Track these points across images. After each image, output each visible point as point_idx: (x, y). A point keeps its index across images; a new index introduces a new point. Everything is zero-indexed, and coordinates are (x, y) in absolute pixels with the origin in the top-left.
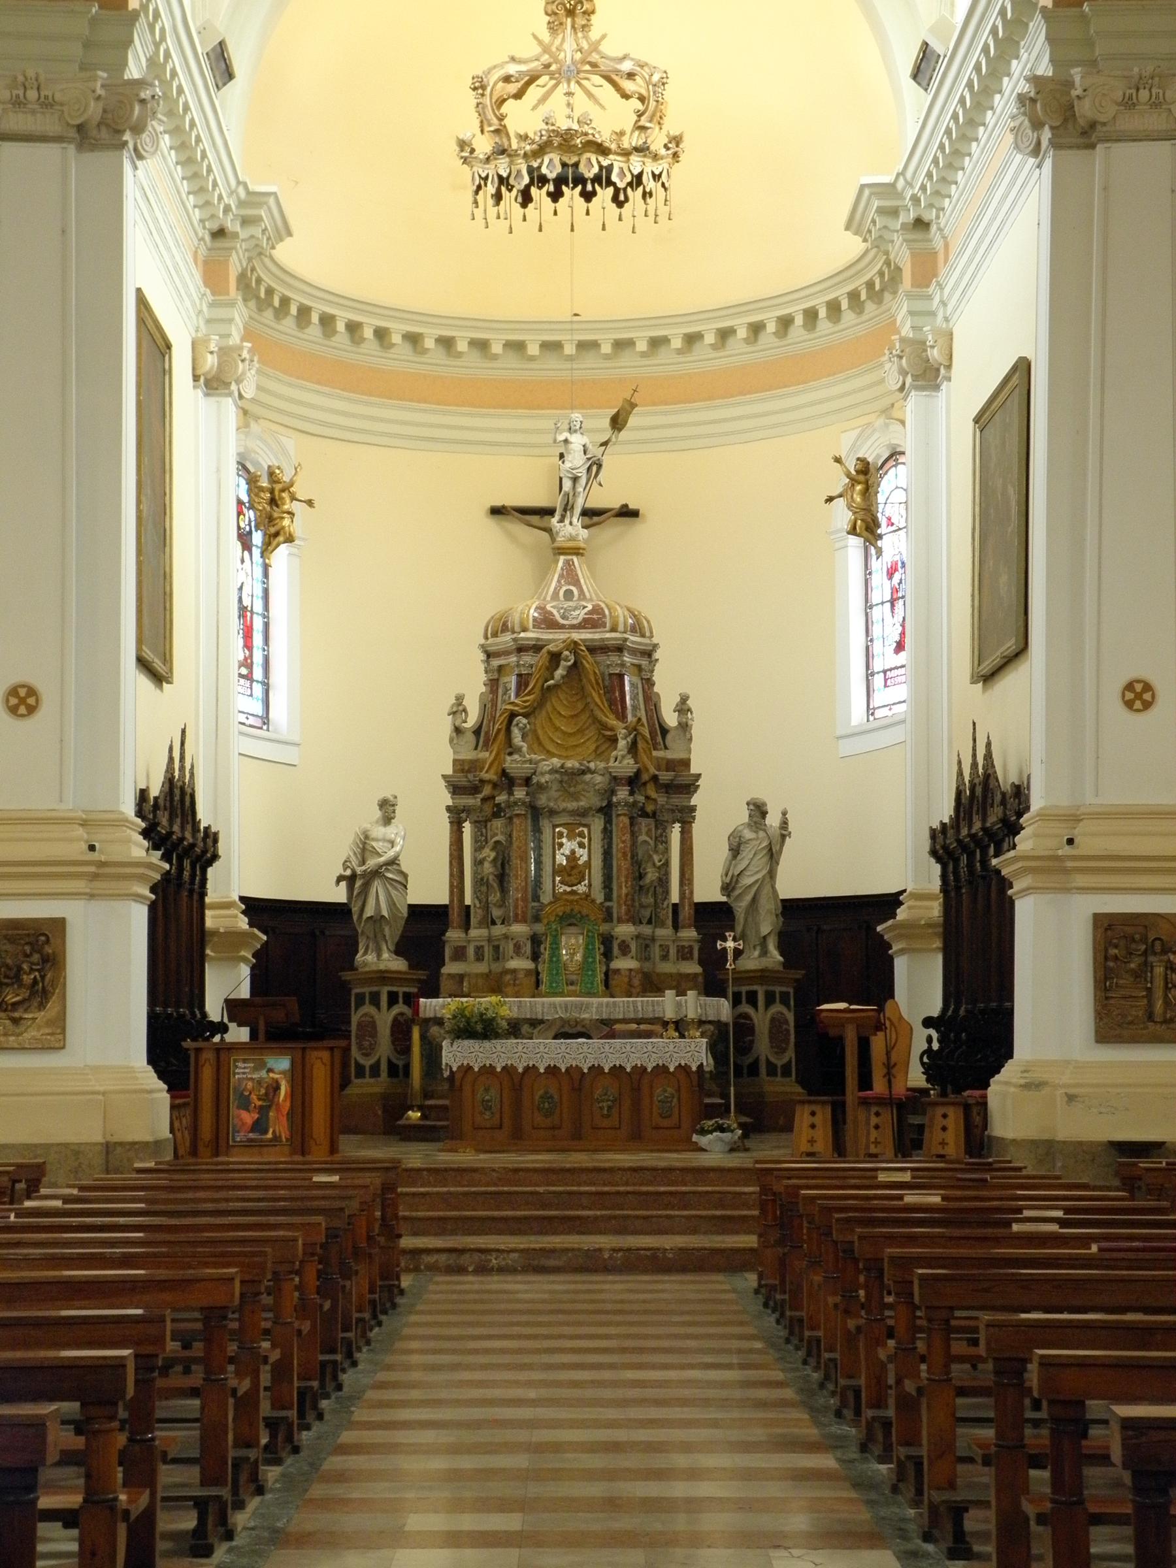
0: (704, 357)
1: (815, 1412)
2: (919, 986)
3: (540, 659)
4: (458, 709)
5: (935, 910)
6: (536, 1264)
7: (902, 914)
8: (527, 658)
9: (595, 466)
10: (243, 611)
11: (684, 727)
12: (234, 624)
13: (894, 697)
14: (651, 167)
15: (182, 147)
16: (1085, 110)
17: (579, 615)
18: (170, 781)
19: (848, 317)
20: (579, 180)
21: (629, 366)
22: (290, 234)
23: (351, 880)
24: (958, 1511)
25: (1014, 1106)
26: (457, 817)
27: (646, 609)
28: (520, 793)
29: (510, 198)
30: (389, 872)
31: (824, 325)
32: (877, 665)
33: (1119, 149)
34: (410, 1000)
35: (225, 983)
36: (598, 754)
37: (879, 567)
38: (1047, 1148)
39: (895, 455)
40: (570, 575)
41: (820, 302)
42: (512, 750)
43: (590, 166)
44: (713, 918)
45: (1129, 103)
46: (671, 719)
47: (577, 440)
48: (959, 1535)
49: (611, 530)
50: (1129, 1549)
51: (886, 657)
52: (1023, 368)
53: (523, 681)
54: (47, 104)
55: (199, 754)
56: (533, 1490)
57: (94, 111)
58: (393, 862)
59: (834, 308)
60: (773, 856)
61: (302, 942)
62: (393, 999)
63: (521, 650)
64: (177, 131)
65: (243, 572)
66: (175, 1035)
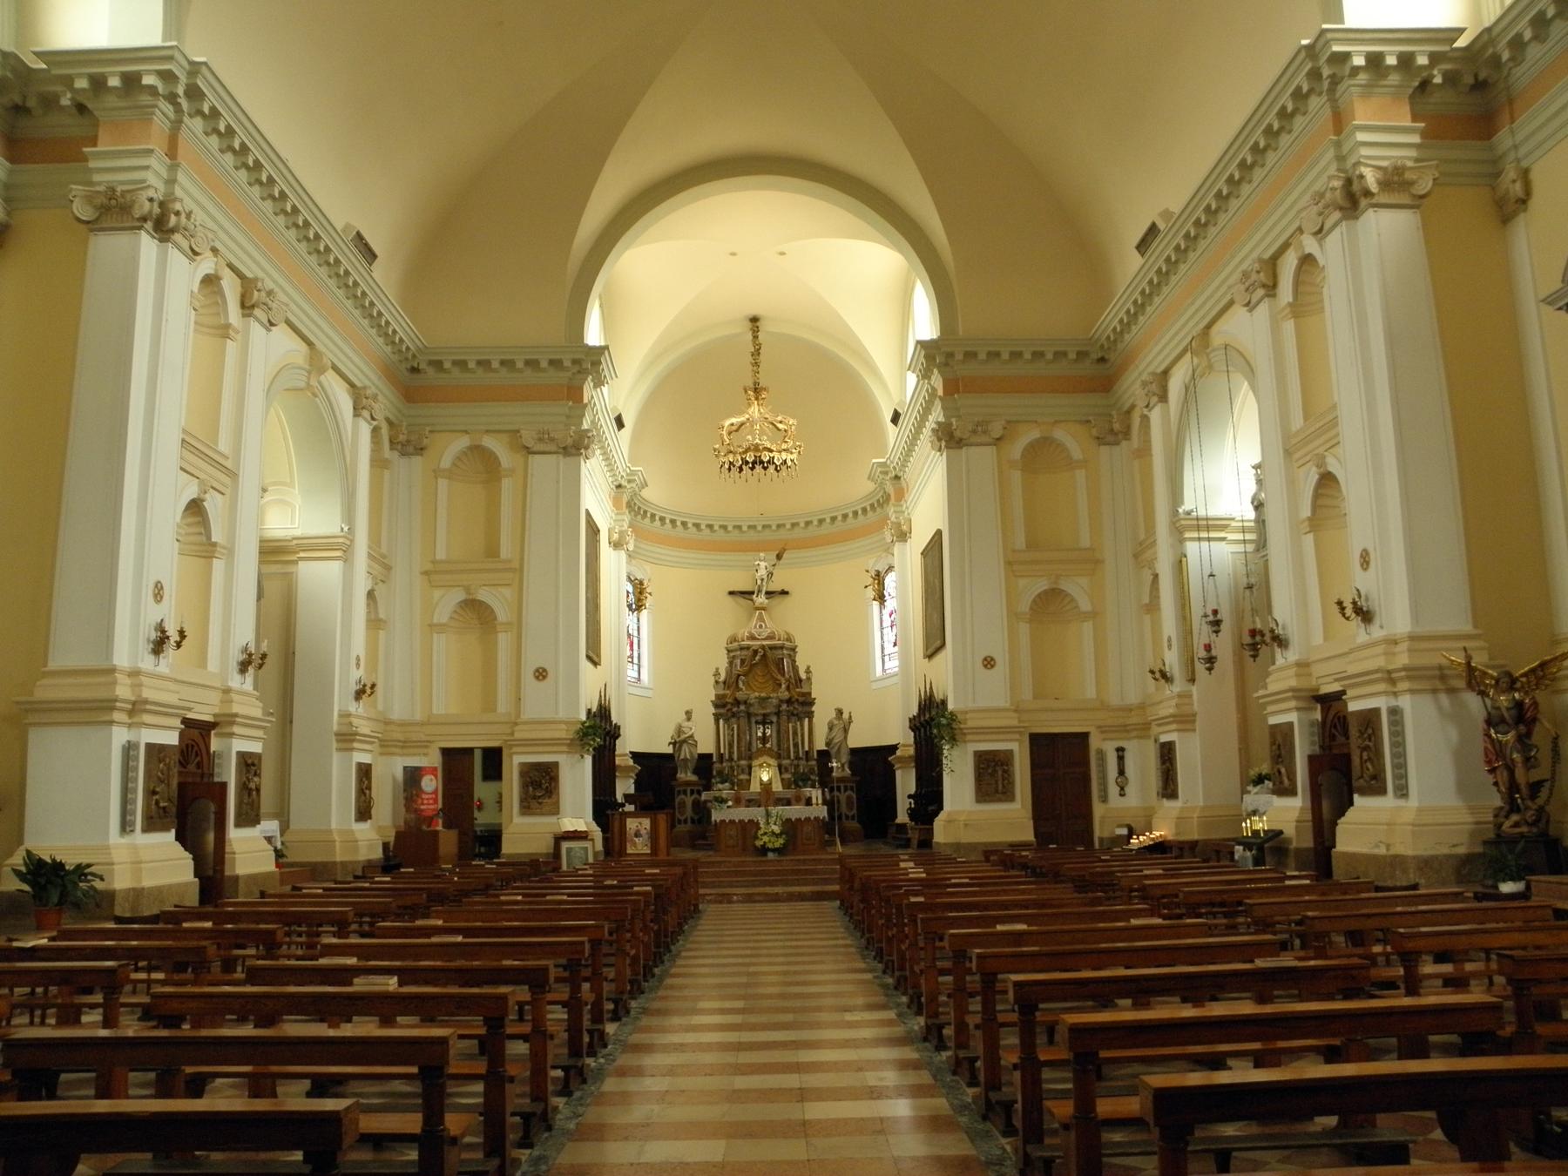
1: (864, 958)
2: (906, 783)
3: (749, 653)
4: (717, 674)
5: (911, 751)
6: (749, 899)
7: (898, 753)
9: (770, 574)
10: (629, 635)
11: (809, 679)
12: (626, 641)
13: (893, 665)
15: (604, 454)
16: (958, 434)
17: (765, 635)
18: (600, 705)
19: (870, 514)
20: (762, 462)
22: (1250, 311)
23: (674, 744)
24: (940, 1027)
25: (942, 832)
26: (717, 717)
28: (742, 707)
29: (735, 471)
30: (690, 741)
31: (861, 517)
33: (973, 449)
34: (699, 793)
35: (624, 786)
36: (774, 691)
37: (886, 612)
38: (958, 846)
39: (890, 568)
40: (761, 619)
41: (859, 508)
42: (738, 689)
43: (766, 457)
44: (824, 756)
45: (974, 432)
46: (803, 676)
48: (940, 1036)
49: (777, 600)
50: (1045, 1086)
51: (889, 649)
52: (939, 533)
53: (743, 661)
54: (552, 440)
55: (612, 694)
56: (750, 991)
57: (570, 441)
58: (692, 736)
59: (864, 510)
60: (846, 731)
61: (654, 769)
62: (692, 792)
63: (742, 649)
64: (602, 448)
65: (630, 620)
66: (604, 807)
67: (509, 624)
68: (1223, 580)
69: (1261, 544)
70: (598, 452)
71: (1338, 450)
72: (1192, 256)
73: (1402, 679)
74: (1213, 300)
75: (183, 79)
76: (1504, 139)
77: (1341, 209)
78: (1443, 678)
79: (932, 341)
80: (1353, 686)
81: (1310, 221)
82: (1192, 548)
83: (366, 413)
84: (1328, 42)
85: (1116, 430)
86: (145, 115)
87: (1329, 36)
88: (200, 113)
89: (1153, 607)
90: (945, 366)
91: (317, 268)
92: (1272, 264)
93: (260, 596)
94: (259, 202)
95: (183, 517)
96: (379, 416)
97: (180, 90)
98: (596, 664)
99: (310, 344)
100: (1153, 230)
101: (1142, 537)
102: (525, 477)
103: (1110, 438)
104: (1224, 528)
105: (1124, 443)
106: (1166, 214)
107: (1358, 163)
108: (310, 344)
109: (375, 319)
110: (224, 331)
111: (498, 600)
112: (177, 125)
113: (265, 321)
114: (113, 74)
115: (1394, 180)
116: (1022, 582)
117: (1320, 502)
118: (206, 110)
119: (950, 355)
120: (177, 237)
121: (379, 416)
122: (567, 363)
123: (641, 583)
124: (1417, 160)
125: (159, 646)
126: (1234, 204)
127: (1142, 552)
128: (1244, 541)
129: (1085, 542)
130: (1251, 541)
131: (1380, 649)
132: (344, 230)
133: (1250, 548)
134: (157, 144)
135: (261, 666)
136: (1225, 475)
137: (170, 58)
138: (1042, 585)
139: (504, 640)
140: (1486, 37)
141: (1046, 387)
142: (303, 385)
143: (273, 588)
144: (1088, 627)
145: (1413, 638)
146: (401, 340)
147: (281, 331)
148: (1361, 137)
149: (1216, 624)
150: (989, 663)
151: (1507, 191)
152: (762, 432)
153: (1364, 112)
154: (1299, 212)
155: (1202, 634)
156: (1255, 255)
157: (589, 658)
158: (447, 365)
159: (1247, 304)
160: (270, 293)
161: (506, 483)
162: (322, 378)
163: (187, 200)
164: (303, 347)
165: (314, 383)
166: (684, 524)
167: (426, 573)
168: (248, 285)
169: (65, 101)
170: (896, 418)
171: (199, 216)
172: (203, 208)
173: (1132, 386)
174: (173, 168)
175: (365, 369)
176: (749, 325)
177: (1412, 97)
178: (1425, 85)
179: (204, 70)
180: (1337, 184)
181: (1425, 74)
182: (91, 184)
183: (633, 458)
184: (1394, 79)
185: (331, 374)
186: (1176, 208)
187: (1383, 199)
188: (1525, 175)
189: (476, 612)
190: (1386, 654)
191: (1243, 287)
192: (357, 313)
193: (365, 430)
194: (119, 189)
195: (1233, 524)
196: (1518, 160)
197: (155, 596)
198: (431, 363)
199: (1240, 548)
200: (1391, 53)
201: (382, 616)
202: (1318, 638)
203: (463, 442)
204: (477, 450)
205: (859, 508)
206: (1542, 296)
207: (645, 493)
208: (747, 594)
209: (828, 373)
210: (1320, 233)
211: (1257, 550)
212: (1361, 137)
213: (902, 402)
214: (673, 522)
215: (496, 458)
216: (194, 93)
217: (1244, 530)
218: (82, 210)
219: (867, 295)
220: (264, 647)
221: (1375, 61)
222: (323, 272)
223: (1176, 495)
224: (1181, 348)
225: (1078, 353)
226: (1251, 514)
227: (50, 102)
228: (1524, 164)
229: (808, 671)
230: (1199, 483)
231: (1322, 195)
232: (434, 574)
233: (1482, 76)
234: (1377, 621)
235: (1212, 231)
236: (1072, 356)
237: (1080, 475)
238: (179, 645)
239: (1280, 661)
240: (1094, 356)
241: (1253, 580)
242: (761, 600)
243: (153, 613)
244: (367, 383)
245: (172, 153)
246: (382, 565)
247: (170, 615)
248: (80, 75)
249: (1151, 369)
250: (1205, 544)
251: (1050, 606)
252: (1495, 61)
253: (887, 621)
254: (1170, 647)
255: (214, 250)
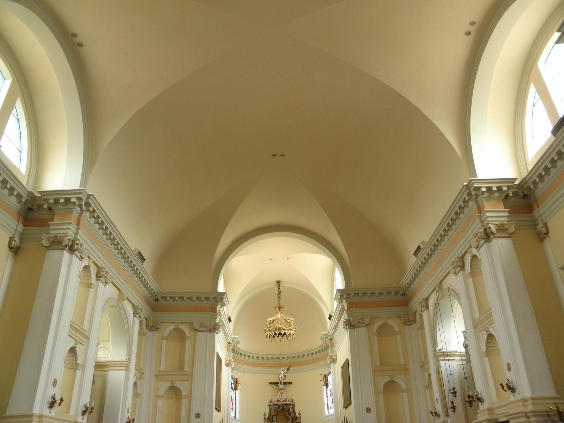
0: (301, 359)
4: (265, 415)
8: (275, 407)
10: (232, 400)
11: (300, 417)
13: (332, 411)
14: (292, 332)
16: (353, 323)
19: (322, 352)
20: (281, 334)
21: (289, 361)
22: (456, 275)
27: (292, 398)
32: (329, 406)
37: (328, 390)
39: (330, 373)
40: (282, 393)
41: (317, 350)
43: (283, 332)
45: (359, 322)
46: (298, 416)
47: (282, 372)
49: (288, 386)
51: (330, 404)
52: (347, 360)
53: (275, 410)
54: (205, 326)
59: (319, 351)
63: (274, 405)
64: (223, 329)
65: (232, 394)
67: (187, 396)
68: (455, 375)
69: (468, 361)
70: (222, 330)
71: (493, 325)
72: (433, 257)
73: (531, 416)
74: (442, 273)
75: (84, 200)
76: (536, 213)
77: (484, 239)
78: (548, 416)
79: (342, 289)
80: (511, 419)
81: (474, 245)
82: (442, 363)
83: (138, 316)
84: (472, 184)
85: (411, 319)
86: (70, 211)
87: (473, 182)
88: (89, 211)
89: (429, 386)
90: (347, 299)
91: (124, 264)
92: (462, 259)
93: (93, 384)
94: (106, 240)
95: (68, 354)
96: (143, 317)
97: (83, 204)
98: (219, 411)
99: (119, 290)
100: (419, 248)
101: (423, 359)
102: (195, 339)
103: (409, 323)
104: (454, 355)
105: (414, 325)
106: (423, 242)
107: (488, 223)
108: (119, 290)
109: (143, 282)
110: (90, 285)
111: (183, 386)
112: (81, 214)
113: (104, 282)
114: (62, 198)
115: (501, 228)
116: (379, 378)
117: (489, 345)
118: (91, 210)
119: (349, 294)
120: (76, 252)
121: (143, 317)
122: (211, 298)
123: (237, 380)
124: (508, 221)
125: (52, 405)
126: (447, 238)
127: (424, 365)
128: (462, 360)
129: (402, 362)
130: (464, 360)
131: (520, 403)
132: (134, 251)
133: (464, 362)
134: (73, 221)
135: (91, 413)
136: (453, 335)
137: (81, 193)
138: (387, 379)
139: (184, 402)
140: (524, 181)
141: (385, 305)
142: (116, 305)
143: (99, 380)
144: (405, 395)
145: (533, 399)
146: (152, 289)
147: (110, 286)
148: (488, 214)
149: (454, 393)
150: (368, 410)
151: (541, 231)
152: (282, 323)
153: (488, 206)
154: (470, 240)
155: (449, 397)
156: (456, 255)
157: (216, 409)
158: (168, 298)
159: (454, 273)
160: (107, 272)
161: (188, 342)
162: (123, 303)
163: (81, 240)
164: (117, 291)
165: (120, 304)
166: (253, 357)
167: (156, 376)
168: (99, 269)
169: (45, 207)
170: (330, 317)
171: (85, 245)
172: (87, 243)
173: (416, 304)
174: (78, 229)
175: (138, 299)
176: (277, 284)
177: (503, 200)
178: (507, 196)
179: (92, 197)
180: (481, 230)
181: (506, 193)
182: (50, 234)
183: (235, 333)
184: (496, 195)
185: (126, 301)
186: (427, 240)
187: (498, 235)
188: (546, 225)
189: (174, 390)
190: (523, 405)
191: (452, 267)
192: (137, 279)
193: (137, 321)
194: (59, 236)
195: (457, 354)
196: (542, 220)
197: (53, 384)
198: (162, 298)
199: (460, 363)
200: (494, 187)
201: (139, 392)
202: (495, 399)
203: (173, 326)
204: (177, 329)
205: (317, 350)
206: (559, 267)
207: (239, 346)
208: (276, 384)
209: (306, 301)
210: (478, 247)
211: (467, 363)
212: (488, 214)
213: (332, 312)
214: (249, 356)
215: (184, 333)
216: (88, 204)
217: (461, 356)
218: (45, 243)
219: (319, 273)
220: (93, 405)
221: (489, 189)
222: (126, 265)
223: (435, 344)
224: (433, 289)
225: (395, 292)
226: (463, 350)
227: (40, 207)
228: (545, 221)
229: (299, 414)
230: (443, 339)
231: (477, 234)
232: (160, 376)
233: (525, 193)
234: (517, 392)
235: (440, 248)
236: (393, 293)
237: (399, 337)
238: (60, 404)
239: (481, 408)
240: (401, 293)
241: (467, 375)
242: (281, 386)
243: (52, 391)
244: (139, 305)
245: (78, 224)
246: (140, 372)
247: (58, 392)
248: (51, 198)
249: (422, 297)
250: (447, 362)
251: (390, 387)
252: (529, 188)
253: (328, 392)
254: (437, 402)
255: (89, 257)
